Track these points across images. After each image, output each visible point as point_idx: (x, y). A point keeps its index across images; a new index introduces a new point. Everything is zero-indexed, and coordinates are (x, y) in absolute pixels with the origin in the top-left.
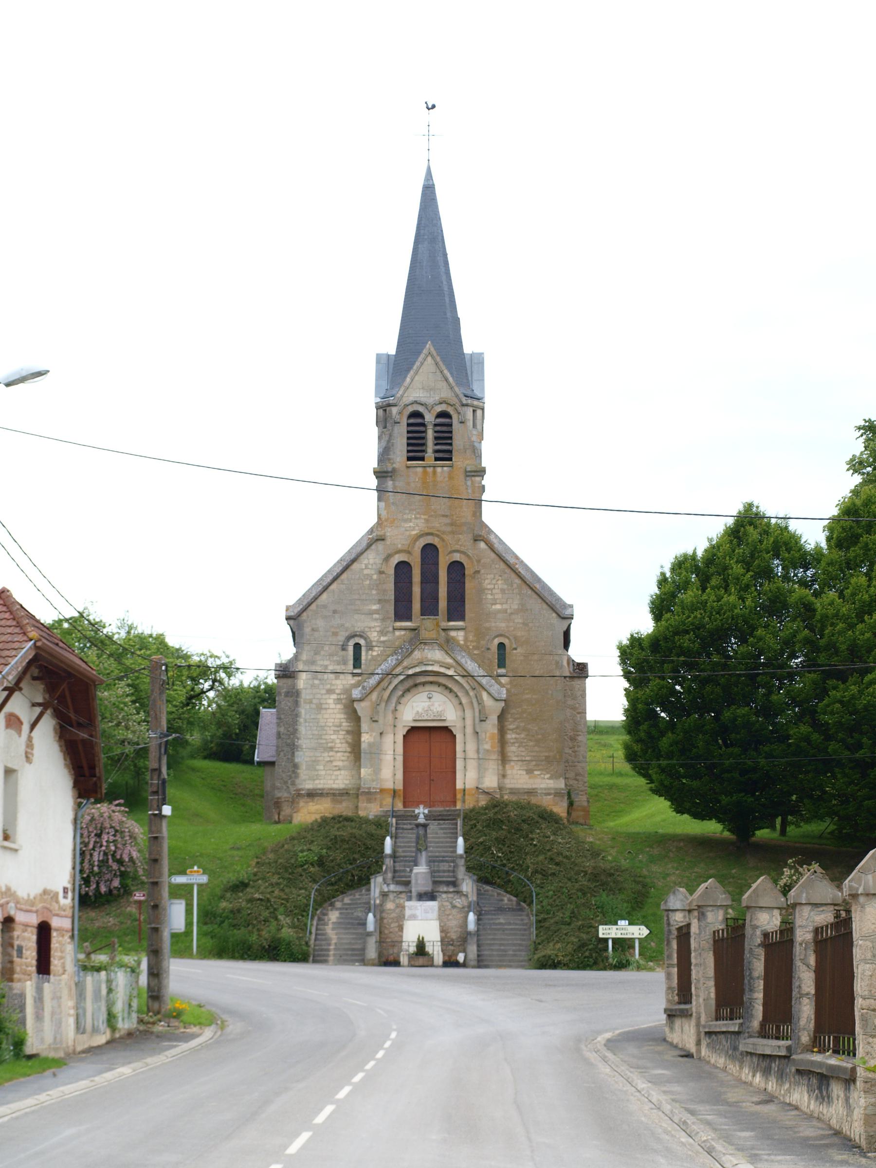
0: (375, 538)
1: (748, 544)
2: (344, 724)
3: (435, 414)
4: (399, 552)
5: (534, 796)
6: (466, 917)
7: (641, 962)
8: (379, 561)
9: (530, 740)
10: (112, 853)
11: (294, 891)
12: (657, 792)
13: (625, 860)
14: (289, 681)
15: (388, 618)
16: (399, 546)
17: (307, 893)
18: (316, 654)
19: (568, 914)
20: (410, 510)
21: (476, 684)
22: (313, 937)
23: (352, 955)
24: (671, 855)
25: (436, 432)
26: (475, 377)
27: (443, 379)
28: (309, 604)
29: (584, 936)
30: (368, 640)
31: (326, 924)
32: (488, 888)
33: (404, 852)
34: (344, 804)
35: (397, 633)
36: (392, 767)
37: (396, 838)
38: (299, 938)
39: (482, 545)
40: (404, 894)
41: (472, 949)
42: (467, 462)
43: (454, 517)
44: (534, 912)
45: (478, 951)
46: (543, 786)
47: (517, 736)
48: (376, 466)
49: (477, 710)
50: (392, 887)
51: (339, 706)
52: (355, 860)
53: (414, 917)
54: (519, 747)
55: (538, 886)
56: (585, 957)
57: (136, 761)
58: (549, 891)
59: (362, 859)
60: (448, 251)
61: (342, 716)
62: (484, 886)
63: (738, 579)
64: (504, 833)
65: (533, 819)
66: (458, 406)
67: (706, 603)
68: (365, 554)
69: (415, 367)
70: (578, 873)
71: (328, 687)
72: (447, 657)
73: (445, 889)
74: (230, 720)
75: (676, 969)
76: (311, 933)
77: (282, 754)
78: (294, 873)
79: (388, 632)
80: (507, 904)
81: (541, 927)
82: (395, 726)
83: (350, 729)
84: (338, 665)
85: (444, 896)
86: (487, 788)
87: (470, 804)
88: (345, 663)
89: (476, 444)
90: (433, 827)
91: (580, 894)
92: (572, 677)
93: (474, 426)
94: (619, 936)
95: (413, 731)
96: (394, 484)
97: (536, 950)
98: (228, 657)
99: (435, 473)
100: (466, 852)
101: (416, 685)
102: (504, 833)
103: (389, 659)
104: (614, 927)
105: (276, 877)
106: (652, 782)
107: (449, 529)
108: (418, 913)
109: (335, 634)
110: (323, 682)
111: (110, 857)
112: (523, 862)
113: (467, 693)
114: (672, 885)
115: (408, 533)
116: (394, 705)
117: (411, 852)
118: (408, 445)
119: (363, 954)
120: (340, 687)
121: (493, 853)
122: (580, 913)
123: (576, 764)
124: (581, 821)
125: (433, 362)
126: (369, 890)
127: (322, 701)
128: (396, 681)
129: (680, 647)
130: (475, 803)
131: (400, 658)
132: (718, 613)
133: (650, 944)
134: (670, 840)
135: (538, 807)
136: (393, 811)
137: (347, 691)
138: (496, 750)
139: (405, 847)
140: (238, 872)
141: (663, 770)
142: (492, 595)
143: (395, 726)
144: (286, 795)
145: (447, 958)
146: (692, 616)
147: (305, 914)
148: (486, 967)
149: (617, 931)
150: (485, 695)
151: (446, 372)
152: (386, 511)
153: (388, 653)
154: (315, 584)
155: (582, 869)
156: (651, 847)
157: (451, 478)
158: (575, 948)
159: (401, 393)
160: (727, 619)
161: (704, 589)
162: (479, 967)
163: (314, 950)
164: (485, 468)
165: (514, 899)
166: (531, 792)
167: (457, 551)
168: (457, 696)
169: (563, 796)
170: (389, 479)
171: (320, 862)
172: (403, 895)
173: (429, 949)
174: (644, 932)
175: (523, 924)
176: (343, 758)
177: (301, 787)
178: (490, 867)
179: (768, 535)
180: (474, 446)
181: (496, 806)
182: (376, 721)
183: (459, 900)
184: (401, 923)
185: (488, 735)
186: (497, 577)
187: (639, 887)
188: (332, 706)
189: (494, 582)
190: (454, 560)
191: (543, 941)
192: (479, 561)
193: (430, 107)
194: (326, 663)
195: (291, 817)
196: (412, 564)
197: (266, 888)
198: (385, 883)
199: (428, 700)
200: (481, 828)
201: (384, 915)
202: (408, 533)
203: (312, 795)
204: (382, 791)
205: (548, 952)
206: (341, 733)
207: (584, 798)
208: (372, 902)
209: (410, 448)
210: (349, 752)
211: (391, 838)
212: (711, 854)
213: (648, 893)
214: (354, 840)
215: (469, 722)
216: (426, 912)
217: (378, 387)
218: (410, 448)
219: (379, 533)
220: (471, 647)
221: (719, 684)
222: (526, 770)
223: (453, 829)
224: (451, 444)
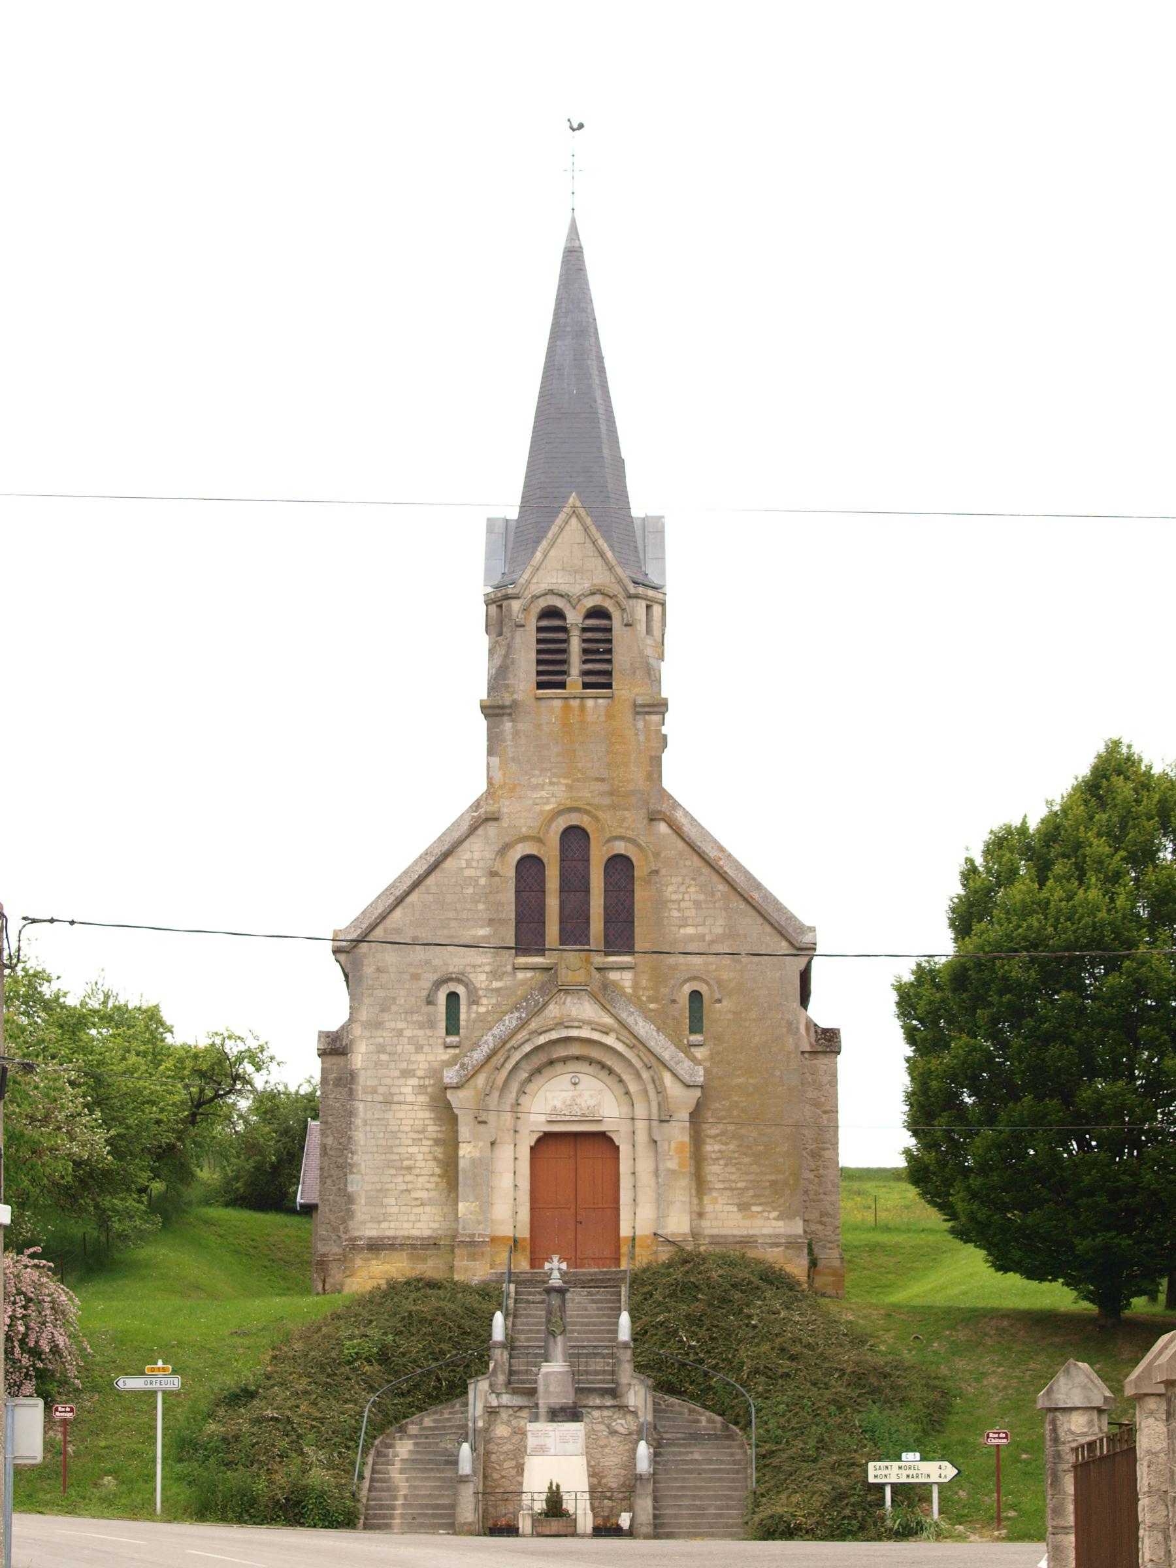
0: (483, 817)
1: (1115, 806)
2: (430, 1128)
3: (584, 611)
4: (523, 839)
5: (751, 1247)
6: (634, 1450)
7: (944, 1525)
8: (489, 854)
9: (745, 1154)
10: (20, 1337)
11: (335, 1405)
12: (962, 1234)
13: (910, 1351)
14: (340, 1060)
16: (524, 830)
17: (358, 1409)
18: (383, 1011)
19: (812, 1443)
21: (652, 1059)
22: (366, 1484)
23: (434, 1516)
24: (989, 1341)
25: (584, 641)
26: (650, 553)
27: (597, 554)
29: (843, 1481)
31: (390, 1463)
32: (672, 1400)
33: (528, 1340)
34: (431, 1263)
35: (521, 975)
36: (512, 1201)
37: (515, 1317)
38: (339, 1486)
39: (663, 828)
40: (527, 1410)
41: (645, 1506)
42: (637, 690)
44: (753, 1441)
45: (655, 1508)
46: (765, 1231)
47: (723, 1148)
48: (485, 697)
49: (654, 1104)
50: (506, 1399)
51: (423, 1099)
52: (443, 1353)
53: (542, 1450)
54: (726, 1165)
55: (758, 1395)
56: (844, 1518)
57: (99, 1199)
58: (779, 1403)
59: (454, 1352)
60: (605, 352)
61: (427, 1115)
62: (666, 1397)
63: (1101, 862)
64: (701, 1305)
65: (750, 1283)
66: (621, 597)
67: (1048, 903)
68: (466, 844)
69: (550, 535)
70: (829, 1372)
71: (404, 1065)
72: (603, 1014)
73: (598, 1402)
74: (262, 1140)
75: (1072, 1538)
76: (361, 1477)
77: (329, 1181)
78: (335, 1374)
79: (504, 973)
80: (705, 1428)
81: (765, 1466)
82: (516, 1131)
83: (440, 1136)
84: (420, 1028)
85: (596, 1413)
86: (673, 1234)
87: (643, 1258)
88: (432, 1025)
89: (652, 661)
90: (576, 1298)
91: (833, 1408)
92: (814, 1053)
93: (649, 631)
94: (904, 1480)
95: (546, 1140)
96: (513, 727)
97: (758, 1506)
98: (257, 1038)
99: (582, 708)
100: (635, 1340)
101: (551, 1063)
102: (701, 1305)
103: (507, 1017)
104: (896, 1464)
105: (305, 1380)
106: (953, 1216)
107: (606, 801)
108: (550, 1442)
109: (416, 977)
110: (396, 1057)
111: (16, 1344)
112: (734, 1356)
113: (638, 1075)
114: (992, 1391)
115: (538, 808)
116: (514, 1095)
117: (538, 1332)
118: (539, 662)
119: (453, 1515)
120: (425, 1065)
121: (681, 1341)
122: (833, 1442)
123: (822, 1196)
124: (832, 1292)
126: (466, 1404)
127: (393, 1090)
128: (517, 1056)
129: (1005, 978)
130: (650, 1258)
131: (524, 1015)
132: (1068, 919)
133: (956, 1493)
134: (985, 1317)
135: (759, 1262)
136: (510, 1273)
137: (436, 1073)
138: (687, 1170)
139: (531, 1331)
140: (238, 1373)
141: (974, 1195)
142: (679, 910)
143: (516, 1131)
144: (336, 1250)
145: (600, 1521)
146: (1025, 924)
147: (352, 1444)
148: (669, 1536)
149: (900, 1472)
150: (668, 1078)
151: (601, 542)
152: (501, 772)
153: (504, 1008)
154: (383, 894)
155: (836, 1365)
156: (954, 1328)
157: (610, 716)
158: (826, 1501)
159: (526, 576)
160: (1085, 928)
161: (1042, 883)
162: (656, 1536)
163: (368, 1507)
164: (666, 699)
165: (718, 1418)
166: (747, 1241)
167: (622, 838)
168: (621, 1081)
169: (799, 1248)
170: (506, 718)
171: (383, 1357)
172: (525, 1413)
173: (568, 1505)
174: (949, 1471)
175: (735, 1462)
176: (428, 1186)
177: (357, 1234)
178: (676, 1365)
179: (1148, 791)
180: (648, 664)
181: (686, 1262)
182: (485, 1122)
183: (623, 1422)
184: (521, 1461)
185: (673, 1145)
186: (688, 881)
187: (935, 1396)
188: (410, 1098)
189: (683, 889)
190: (616, 852)
191: (768, 1491)
192: (657, 855)
193: (575, 126)
194: (401, 1025)
195: (342, 1285)
196: (545, 861)
197: (287, 1399)
198: (493, 1392)
199: (572, 1087)
200: (661, 1299)
201: (491, 1447)
202: (538, 808)
203: (376, 1247)
204: (494, 1240)
205: (779, 1510)
206: (425, 1142)
207: (835, 1253)
208: (470, 1424)
209: (542, 668)
210: (439, 1176)
211: (506, 1317)
212: (1056, 1340)
213: (951, 1405)
214: (440, 1318)
215: (641, 1126)
216: (564, 1441)
217: (488, 570)
218: (542, 668)
219: (489, 809)
220: (644, 999)
221: (1072, 1043)
222: (738, 1205)
223: (613, 1301)
224: (610, 661)
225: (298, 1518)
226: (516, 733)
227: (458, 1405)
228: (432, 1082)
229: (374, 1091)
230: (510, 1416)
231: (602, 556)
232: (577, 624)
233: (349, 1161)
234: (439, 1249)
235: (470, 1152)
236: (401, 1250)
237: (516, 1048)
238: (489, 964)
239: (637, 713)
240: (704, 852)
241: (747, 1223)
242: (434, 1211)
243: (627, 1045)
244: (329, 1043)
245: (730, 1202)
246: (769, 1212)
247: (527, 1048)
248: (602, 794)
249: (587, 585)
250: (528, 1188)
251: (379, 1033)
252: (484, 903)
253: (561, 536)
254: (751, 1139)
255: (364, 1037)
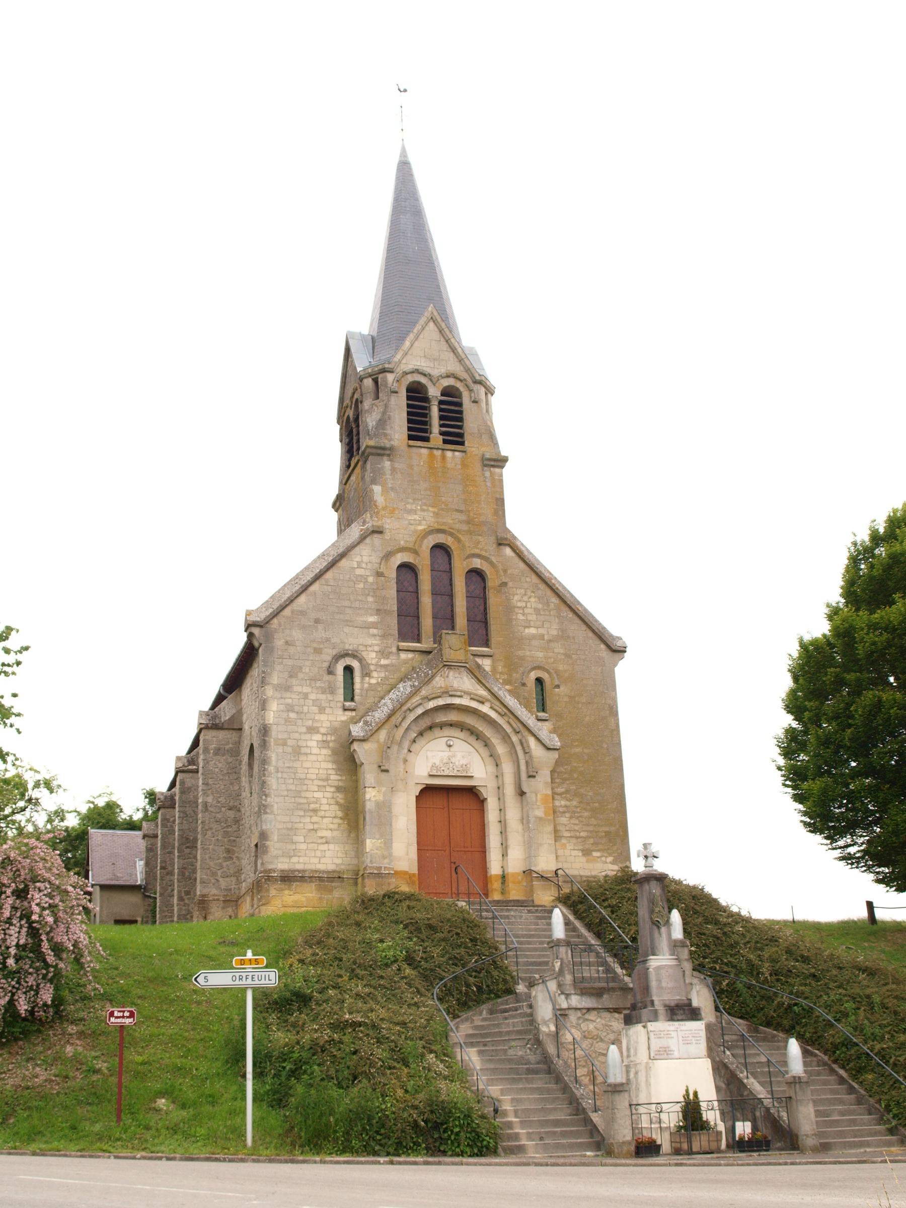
0: (371, 529)
2: (332, 777)
8: (375, 559)
9: (585, 809)
15: (390, 634)
16: (402, 543)
18: (291, 677)
20: (414, 500)
27: (449, 349)
28: (283, 608)
30: (364, 662)
34: (337, 894)
35: (403, 656)
39: (508, 551)
42: (483, 449)
43: (471, 514)
47: (568, 803)
50: (575, 1001)
51: (325, 752)
54: (571, 818)
61: (330, 766)
68: (357, 549)
69: (415, 331)
71: (310, 723)
72: (479, 687)
77: (209, 833)
79: (391, 653)
83: (341, 784)
84: (323, 693)
88: (332, 691)
95: (428, 792)
96: (392, 465)
99: (444, 457)
101: (430, 728)
107: (465, 527)
108: (673, 1043)
110: (302, 716)
115: (412, 528)
120: (327, 724)
125: (436, 329)
127: (301, 743)
128: (412, 717)
131: (416, 684)
142: (523, 614)
154: (288, 583)
157: (464, 465)
167: (478, 556)
170: (385, 458)
176: (332, 826)
177: (270, 867)
182: (387, 771)
186: (529, 593)
189: (525, 598)
192: (505, 571)
194: (306, 690)
198: (562, 993)
202: (412, 528)
203: (288, 878)
206: (328, 789)
210: (341, 818)
222: (582, 851)
224: (461, 427)
225: (437, 1144)
226: (393, 470)
227: (484, 1012)
228: (333, 738)
229: (284, 744)
230: (579, 1018)
231: (453, 352)
232: (437, 397)
233: (264, 802)
234: (343, 881)
235: (374, 796)
236: (310, 882)
237: (410, 710)
238: (377, 645)
239: (485, 466)
240: (541, 572)
241: (590, 866)
242: (337, 849)
243: (499, 714)
244: (210, 720)
245: (576, 848)
246: (606, 857)
247: (420, 711)
248: (461, 522)
249: (443, 371)
250: (416, 831)
251: (288, 695)
252: (373, 596)
253: (422, 334)
254: (589, 797)
255: (275, 698)
